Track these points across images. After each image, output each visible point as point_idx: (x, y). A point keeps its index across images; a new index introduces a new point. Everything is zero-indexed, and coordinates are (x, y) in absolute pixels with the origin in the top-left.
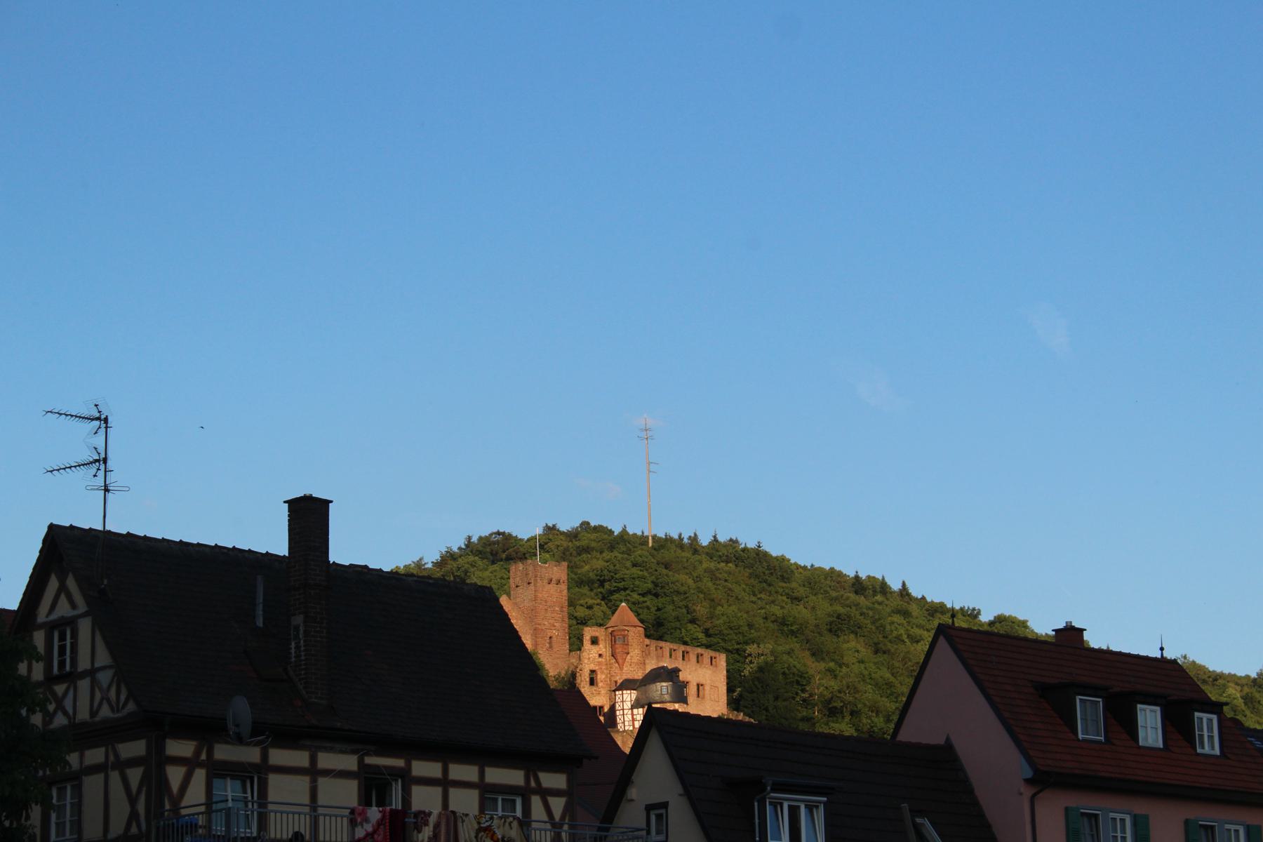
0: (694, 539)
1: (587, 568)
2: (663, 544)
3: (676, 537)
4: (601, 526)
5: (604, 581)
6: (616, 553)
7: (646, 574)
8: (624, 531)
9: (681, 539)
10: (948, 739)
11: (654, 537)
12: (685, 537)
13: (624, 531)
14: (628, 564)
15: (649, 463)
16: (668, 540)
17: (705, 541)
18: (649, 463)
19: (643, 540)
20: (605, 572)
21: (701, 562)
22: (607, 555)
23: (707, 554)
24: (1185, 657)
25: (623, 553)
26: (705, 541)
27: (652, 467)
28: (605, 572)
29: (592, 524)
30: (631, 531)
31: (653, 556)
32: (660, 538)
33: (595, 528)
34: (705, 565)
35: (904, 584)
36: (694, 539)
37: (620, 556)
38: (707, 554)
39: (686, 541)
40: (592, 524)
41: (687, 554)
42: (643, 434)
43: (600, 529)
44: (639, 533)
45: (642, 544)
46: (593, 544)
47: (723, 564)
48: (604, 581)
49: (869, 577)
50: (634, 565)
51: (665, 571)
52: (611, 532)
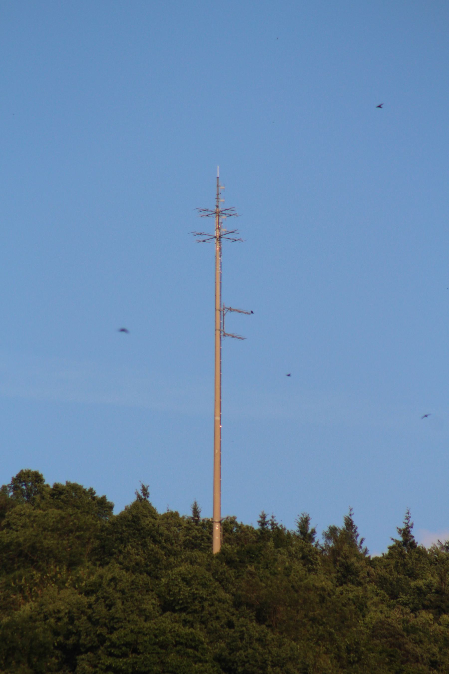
0: (345, 537)
1: (27, 609)
2: (256, 546)
3: (291, 527)
4: (75, 488)
5: (77, 649)
6: (114, 570)
7: (200, 633)
8: (142, 505)
9: (306, 533)
10: (349, 524)
11: (229, 526)
12: (320, 528)
13: (142, 505)
14: (150, 603)
15: (223, 311)
16: (270, 536)
17: (376, 543)
18: (223, 311)
19: (196, 531)
20: (82, 623)
21: (361, 606)
22: (87, 573)
23: (382, 582)
24: (323, 538)
25: (136, 568)
26: (376, 543)
27: (232, 323)
28: (82, 623)
29: (50, 481)
30: (160, 505)
31: (222, 581)
32: (245, 531)
33: (58, 491)
34: (374, 615)
35: (145, 490)
36: (345, 537)
37: (127, 577)
38: (382, 582)
39: (320, 540)
40: (50, 481)
41: (322, 580)
42: (210, 226)
43: (71, 496)
44: (186, 513)
45: (192, 545)
46: (49, 542)
47: (426, 616)
48: (77, 649)
49: (68, 484)
50: (167, 607)
51: (255, 629)
52: (104, 505)
